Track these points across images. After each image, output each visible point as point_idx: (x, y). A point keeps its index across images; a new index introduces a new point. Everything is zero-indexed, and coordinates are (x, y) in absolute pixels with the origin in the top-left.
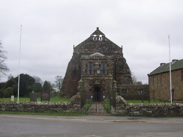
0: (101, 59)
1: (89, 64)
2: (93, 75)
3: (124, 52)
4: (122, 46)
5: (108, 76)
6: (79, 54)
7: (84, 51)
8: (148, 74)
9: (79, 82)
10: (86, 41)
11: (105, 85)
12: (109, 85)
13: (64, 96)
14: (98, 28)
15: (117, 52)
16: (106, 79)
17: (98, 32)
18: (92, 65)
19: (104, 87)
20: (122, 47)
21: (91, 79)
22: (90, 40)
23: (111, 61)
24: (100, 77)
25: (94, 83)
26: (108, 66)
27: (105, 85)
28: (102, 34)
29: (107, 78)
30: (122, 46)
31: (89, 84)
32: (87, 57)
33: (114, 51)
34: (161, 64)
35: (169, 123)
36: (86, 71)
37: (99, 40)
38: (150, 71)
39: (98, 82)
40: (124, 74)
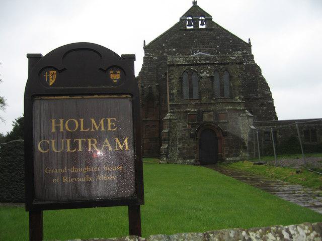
0: (213, 64)
3: (254, 51)
4: (249, 39)
9: (165, 118)
12: (237, 124)
14: (195, 3)
16: (229, 110)
17: (195, 12)
20: (250, 43)
22: (179, 28)
24: (214, 104)
27: (228, 122)
28: (203, 13)
29: (230, 107)
30: (249, 39)
32: (181, 60)
36: (180, 92)
37: (188, 27)
40: (257, 99)
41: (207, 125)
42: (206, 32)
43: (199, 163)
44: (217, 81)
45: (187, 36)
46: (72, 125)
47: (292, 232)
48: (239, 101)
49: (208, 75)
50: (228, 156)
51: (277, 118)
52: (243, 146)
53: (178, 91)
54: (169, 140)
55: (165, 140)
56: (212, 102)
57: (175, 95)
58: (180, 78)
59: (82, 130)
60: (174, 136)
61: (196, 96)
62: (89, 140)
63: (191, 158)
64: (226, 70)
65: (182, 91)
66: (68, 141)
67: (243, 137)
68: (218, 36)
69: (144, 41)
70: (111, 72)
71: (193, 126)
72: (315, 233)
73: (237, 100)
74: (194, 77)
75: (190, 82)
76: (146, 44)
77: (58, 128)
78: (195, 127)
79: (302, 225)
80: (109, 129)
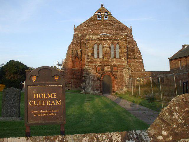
1: (96, 47)
2: (101, 60)
3: (134, 33)
4: (131, 27)
5: (120, 61)
8: (169, 59)
10: (90, 20)
11: (117, 72)
12: (122, 73)
14: (102, 5)
15: (126, 33)
16: (118, 65)
17: (102, 11)
19: (116, 75)
20: (131, 28)
23: (124, 41)
25: (103, 69)
26: (120, 49)
29: (119, 63)
30: (131, 27)
31: (97, 72)
32: (94, 37)
33: (122, 32)
34: (184, 46)
35: (42, 112)
38: (172, 53)
39: (108, 68)
41: (106, 73)
42: (108, 21)
43: (101, 93)
44: (112, 50)
46: (41, 96)
47: (112, 135)
48: (124, 60)
49: (108, 46)
51: (144, 70)
53: (92, 54)
54: (86, 81)
55: (84, 80)
58: (93, 47)
59: (45, 97)
60: (89, 78)
62: (47, 101)
63: (97, 90)
64: (118, 44)
65: (94, 54)
66: (40, 101)
69: (74, 25)
70: (55, 77)
72: (119, 135)
73: (123, 60)
74: (101, 46)
75: (98, 50)
77: (36, 97)
79: (116, 132)
80: (54, 97)
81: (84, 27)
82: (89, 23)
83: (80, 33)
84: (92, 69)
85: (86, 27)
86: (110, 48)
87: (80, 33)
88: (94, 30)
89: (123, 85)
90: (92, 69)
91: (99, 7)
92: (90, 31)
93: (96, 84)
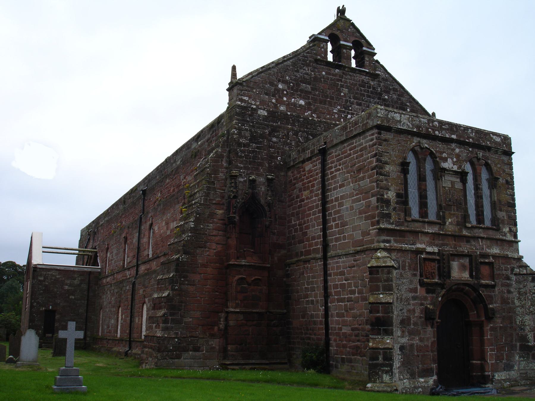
1: (411, 158)
6: (265, 118)
7: (288, 105)
11: (493, 287)
12: (509, 292)
13: (185, 355)
14: (341, 12)
18: (429, 166)
21: (433, 253)
24: (468, 239)
27: (493, 287)
29: (495, 250)
45: (328, 78)
49: (455, 168)
50: (495, 369)
52: (521, 346)
53: (398, 195)
56: (465, 233)
57: (393, 205)
61: (432, 216)
63: (426, 373)
67: (523, 323)
68: (387, 92)
69: (234, 68)
71: (430, 288)
76: (239, 76)
78: (433, 292)
81: (279, 81)
82: (298, 71)
83: (263, 102)
84: (404, 268)
85: (284, 82)
86: (463, 175)
87: (263, 102)
88: (315, 100)
89: (512, 347)
90: (404, 268)
91: (331, 18)
92: (302, 102)
93: (421, 340)
